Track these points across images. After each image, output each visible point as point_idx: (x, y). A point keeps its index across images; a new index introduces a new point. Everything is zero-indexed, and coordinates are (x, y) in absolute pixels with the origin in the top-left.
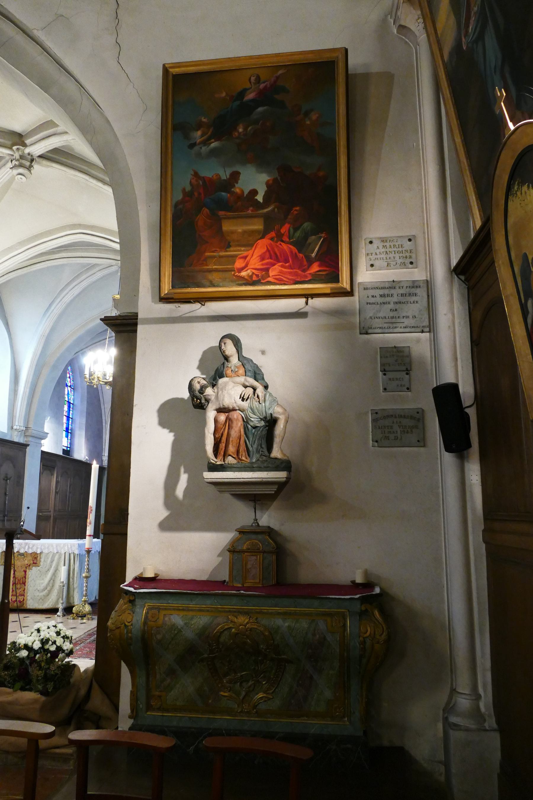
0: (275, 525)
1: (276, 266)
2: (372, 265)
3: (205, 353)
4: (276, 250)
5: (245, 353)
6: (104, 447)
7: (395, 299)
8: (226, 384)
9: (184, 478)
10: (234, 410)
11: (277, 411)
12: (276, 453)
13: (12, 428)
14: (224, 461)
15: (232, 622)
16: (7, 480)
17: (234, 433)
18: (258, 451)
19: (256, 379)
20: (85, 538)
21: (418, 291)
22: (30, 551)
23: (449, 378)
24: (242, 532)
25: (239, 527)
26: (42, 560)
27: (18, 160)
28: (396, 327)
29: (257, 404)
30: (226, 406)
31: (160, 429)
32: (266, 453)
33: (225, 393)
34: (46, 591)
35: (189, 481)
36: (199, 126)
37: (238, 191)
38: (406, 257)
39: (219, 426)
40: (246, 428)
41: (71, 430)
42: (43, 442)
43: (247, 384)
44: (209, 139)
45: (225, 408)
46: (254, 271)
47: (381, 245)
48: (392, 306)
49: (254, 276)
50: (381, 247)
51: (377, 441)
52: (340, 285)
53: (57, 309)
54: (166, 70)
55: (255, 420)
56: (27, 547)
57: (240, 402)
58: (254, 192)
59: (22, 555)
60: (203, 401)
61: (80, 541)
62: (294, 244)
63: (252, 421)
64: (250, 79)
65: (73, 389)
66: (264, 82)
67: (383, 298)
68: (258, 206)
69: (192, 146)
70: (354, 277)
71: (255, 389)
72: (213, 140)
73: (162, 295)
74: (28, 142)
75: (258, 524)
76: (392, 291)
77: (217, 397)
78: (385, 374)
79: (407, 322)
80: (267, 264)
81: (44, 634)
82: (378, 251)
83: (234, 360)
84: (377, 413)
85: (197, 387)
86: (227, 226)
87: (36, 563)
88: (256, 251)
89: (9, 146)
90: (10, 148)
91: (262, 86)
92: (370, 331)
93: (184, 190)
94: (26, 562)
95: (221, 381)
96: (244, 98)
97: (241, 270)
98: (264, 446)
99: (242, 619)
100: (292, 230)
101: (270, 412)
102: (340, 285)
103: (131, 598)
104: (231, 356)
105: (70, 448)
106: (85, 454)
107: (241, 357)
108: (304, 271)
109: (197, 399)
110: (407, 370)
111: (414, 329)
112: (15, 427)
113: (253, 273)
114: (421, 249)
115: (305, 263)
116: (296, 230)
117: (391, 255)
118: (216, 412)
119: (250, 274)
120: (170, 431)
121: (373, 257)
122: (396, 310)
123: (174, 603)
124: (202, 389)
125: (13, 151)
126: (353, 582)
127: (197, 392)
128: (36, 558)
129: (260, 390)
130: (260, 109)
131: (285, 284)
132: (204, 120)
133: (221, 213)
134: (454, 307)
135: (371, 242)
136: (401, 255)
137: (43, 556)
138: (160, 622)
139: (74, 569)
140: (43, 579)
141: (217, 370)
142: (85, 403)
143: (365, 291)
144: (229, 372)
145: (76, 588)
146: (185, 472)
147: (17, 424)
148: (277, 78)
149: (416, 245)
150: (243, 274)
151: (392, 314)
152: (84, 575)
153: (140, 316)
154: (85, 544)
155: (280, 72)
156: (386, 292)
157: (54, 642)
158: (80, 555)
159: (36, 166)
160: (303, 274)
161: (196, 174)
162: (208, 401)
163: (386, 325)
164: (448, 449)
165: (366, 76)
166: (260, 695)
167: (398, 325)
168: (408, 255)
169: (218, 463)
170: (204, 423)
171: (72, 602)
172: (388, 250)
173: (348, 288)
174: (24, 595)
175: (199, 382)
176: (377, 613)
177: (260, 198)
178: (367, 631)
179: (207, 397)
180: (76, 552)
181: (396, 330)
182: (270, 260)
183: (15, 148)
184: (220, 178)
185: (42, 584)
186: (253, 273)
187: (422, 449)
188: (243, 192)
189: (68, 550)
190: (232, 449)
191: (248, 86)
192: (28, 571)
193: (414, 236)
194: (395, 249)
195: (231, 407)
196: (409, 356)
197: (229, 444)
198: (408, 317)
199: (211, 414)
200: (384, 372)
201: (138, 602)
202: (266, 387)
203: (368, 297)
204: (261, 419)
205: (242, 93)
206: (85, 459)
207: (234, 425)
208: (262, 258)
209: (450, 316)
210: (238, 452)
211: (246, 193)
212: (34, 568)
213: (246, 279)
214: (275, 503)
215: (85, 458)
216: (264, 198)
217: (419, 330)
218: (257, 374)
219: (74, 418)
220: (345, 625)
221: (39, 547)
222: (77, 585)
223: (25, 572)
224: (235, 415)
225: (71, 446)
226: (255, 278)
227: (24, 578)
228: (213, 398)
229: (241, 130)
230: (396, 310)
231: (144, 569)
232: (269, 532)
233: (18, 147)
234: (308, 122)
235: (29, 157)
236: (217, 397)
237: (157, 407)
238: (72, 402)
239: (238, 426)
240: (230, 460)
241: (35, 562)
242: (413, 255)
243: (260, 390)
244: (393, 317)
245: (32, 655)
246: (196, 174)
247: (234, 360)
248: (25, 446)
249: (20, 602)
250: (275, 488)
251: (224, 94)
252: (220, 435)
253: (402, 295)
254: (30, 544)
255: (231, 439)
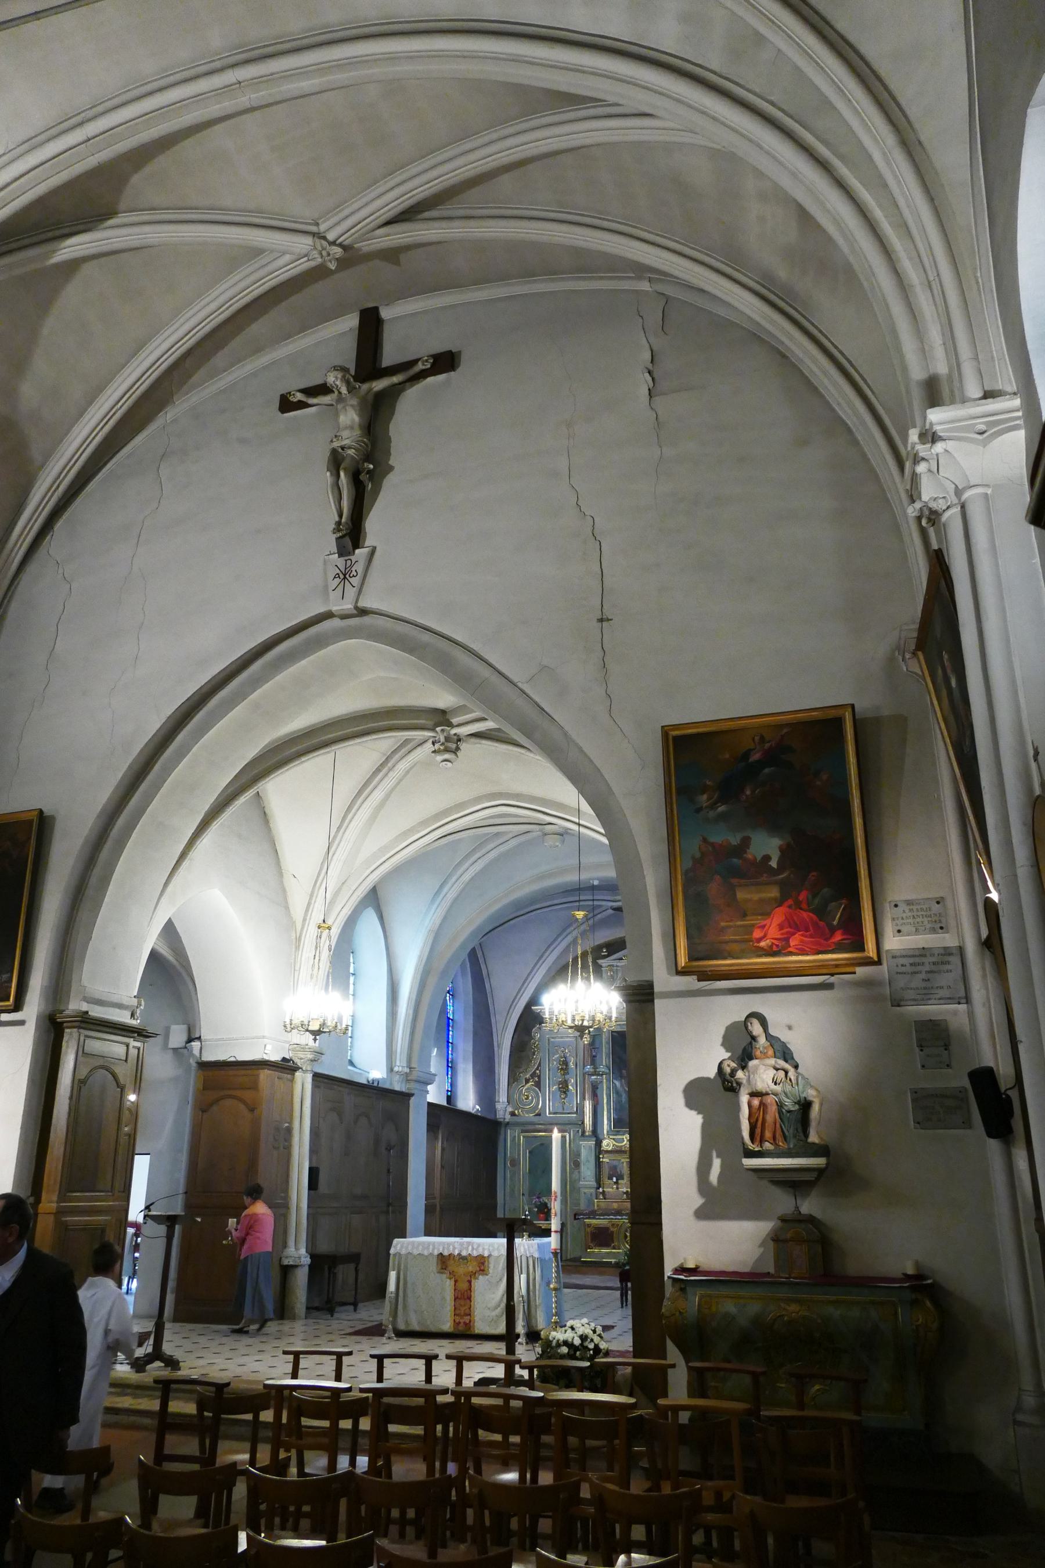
0: (817, 1214)
1: (797, 935)
2: (899, 931)
3: (728, 1029)
4: (795, 918)
5: (772, 1031)
6: (497, 1087)
7: (927, 968)
8: (756, 1068)
9: (717, 1164)
10: (767, 1094)
11: (811, 1094)
12: (813, 1138)
13: (391, 1070)
14: (761, 1147)
15: (784, 1309)
16: (390, 1150)
17: (769, 1118)
18: (795, 1136)
19: (786, 1061)
20: (550, 1236)
21: (951, 959)
22: (475, 1254)
23: (988, 1061)
24: (783, 1220)
25: (780, 1215)
26: (491, 1266)
27: (443, 744)
28: (930, 999)
29: (790, 1087)
30: (759, 1090)
31: (687, 1110)
32: (803, 1138)
33: (757, 1077)
34: (499, 1309)
35: (722, 1166)
36: (704, 790)
37: (750, 856)
38: (935, 922)
39: (754, 1111)
40: (780, 1112)
41: (452, 1062)
42: (429, 1087)
43: (778, 1067)
44: (716, 803)
45: (759, 1093)
46: (773, 941)
47: (907, 908)
48: (923, 976)
49: (774, 946)
50: (907, 911)
51: (919, 1123)
52: (866, 954)
53: (451, 892)
54: (665, 731)
55: (789, 1104)
56: (470, 1248)
57: (773, 1086)
58: (767, 858)
59: (464, 1258)
60: (735, 1085)
61: (546, 1240)
62: (813, 911)
63: (786, 1105)
64: (753, 739)
65: (452, 995)
66: (769, 742)
67: (913, 967)
68: (773, 872)
69: (699, 810)
70: (881, 945)
71: (786, 1073)
72: (719, 804)
73: (679, 969)
74: (455, 721)
75: (800, 1212)
76: (923, 960)
77: (749, 1080)
78: (922, 1050)
79: (942, 993)
80: (787, 933)
81: (581, 1331)
82: (904, 915)
83: (762, 1040)
84: (916, 1092)
85: (728, 1070)
86: (741, 895)
87: (483, 1270)
88: (774, 920)
89: (431, 727)
90: (433, 730)
91: (767, 746)
92: (902, 1003)
93: (693, 858)
94: (471, 1269)
95: (752, 1063)
96: (748, 759)
97: (759, 940)
98: (800, 1130)
99: (793, 1307)
100: (810, 897)
101: (804, 1096)
102: (866, 954)
103: (683, 1286)
104: (759, 1036)
105: (451, 1091)
106: (474, 1102)
107: (768, 1036)
108: (827, 939)
109: (728, 1082)
110: (946, 1045)
111: (950, 1000)
112: (396, 1069)
113: (773, 943)
114: (951, 913)
115: (827, 931)
116: (814, 896)
117: (918, 920)
118: (748, 1096)
119: (770, 944)
120: (699, 1113)
121: (900, 922)
122: (929, 980)
123: (724, 1291)
124: (733, 1072)
125: (437, 732)
126: (905, 1275)
127: (728, 1076)
128: (483, 1264)
129: (792, 1074)
130: (767, 770)
131: (808, 954)
132: (708, 783)
133: (735, 881)
134: (987, 983)
135: (896, 906)
136: (930, 919)
137: (492, 1260)
138: (714, 1309)
139: (534, 1279)
140: (494, 1293)
141: (744, 1049)
142: (471, 1017)
143: (894, 960)
144: (758, 1053)
145: (539, 1305)
146: (718, 1156)
147: (398, 1063)
148: (782, 736)
149: (945, 906)
150: (763, 944)
151: (924, 984)
152: (552, 1286)
153: (657, 989)
154: (550, 1243)
155: (785, 731)
156: (917, 960)
157: (592, 1340)
158: (542, 1260)
159: (463, 746)
160: (826, 942)
161: (705, 840)
162: (739, 1084)
163: (918, 997)
164: (990, 1135)
165: (877, 721)
166: (817, 1387)
167: (931, 996)
168: (937, 918)
169: (756, 1149)
170: (737, 1108)
171: (534, 1325)
172: (915, 914)
173: (876, 959)
174: (470, 1315)
175: (729, 1066)
176: (928, 1304)
177: (774, 864)
178: (919, 1319)
179: (738, 1080)
180: (536, 1255)
181: (930, 1002)
182: (789, 929)
183: (438, 729)
184: (730, 843)
185: (493, 1299)
186: (773, 943)
187: (968, 1132)
188: (755, 859)
189: (525, 1251)
190: (768, 1134)
191: (752, 746)
192: (473, 1281)
193: (942, 898)
194: (923, 913)
195: (764, 1091)
196: (946, 1030)
197: (765, 1128)
198: (942, 988)
199: (744, 1099)
200: (921, 1047)
201: (689, 1290)
202: (796, 1067)
203: (897, 966)
204: (795, 1103)
205: (746, 755)
206: (475, 1110)
207: (769, 1110)
208: (781, 927)
209: (983, 992)
210: (774, 1138)
211: (759, 858)
212: (480, 1276)
213: (765, 950)
214: (814, 1193)
215: (474, 1107)
216: (778, 864)
217: (957, 1001)
218: (785, 1054)
219: (454, 1042)
220: (896, 1313)
221: (486, 1247)
222: (540, 1302)
223: (470, 1282)
224: (770, 1100)
225: (453, 1089)
226: (775, 948)
227: (469, 1291)
228: (744, 1082)
229: (748, 792)
230: (929, 980)
231: (685, 1259)
232: (811, 1220)
233: (442, 728)
234: (818, 783)
235: (455, 737)
236: (749, 1080)
237: (682, 1087)
238: (451, 1017)
239: (772, 1111)
240: (768, 1146)
241: (482, 1268)
242: (943, 919)
243: (792, 1074)
244: (925, 988)
245: (572, 1352)
246: (705, 840)
247: (762, 1040)
248: (406, 1096)
249: (465, 1323)
250: (815, 1174)
251: (727, 756)
252: (755, 1120)
253: (934, 963)
254: (473, 1243)
255: (767, 1124)
